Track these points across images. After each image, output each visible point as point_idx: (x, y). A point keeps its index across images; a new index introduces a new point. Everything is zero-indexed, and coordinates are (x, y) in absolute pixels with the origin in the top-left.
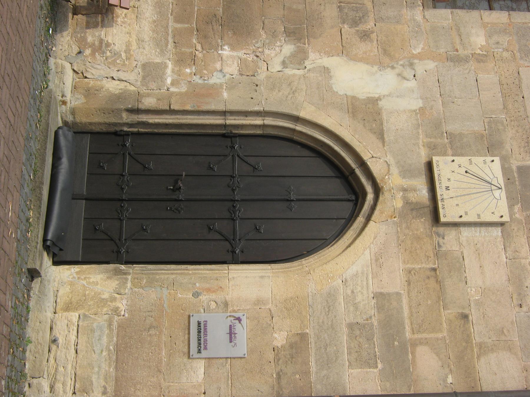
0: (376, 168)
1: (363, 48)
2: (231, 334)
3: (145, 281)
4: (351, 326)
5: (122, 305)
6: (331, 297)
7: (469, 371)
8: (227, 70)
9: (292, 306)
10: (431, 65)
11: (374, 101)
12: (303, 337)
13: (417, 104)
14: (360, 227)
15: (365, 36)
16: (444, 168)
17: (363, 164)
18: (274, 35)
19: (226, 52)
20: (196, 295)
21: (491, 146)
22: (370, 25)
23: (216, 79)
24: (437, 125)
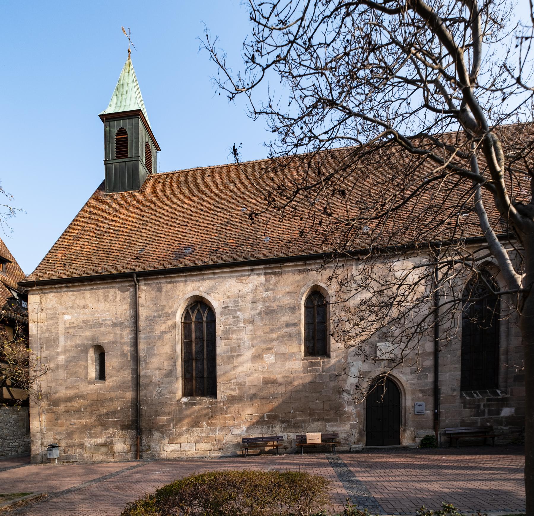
2: (420, 405)
4: (418, 380)
5: (412, 429)
6: (411, 384)
7: (429, 354)
8: (351, 409)
9: (413, 392)
12: (420, 390)
14: (382, 472)
18: (341, 398)
19: (346, 409)
20: (410, 413)
23: (354, 411)
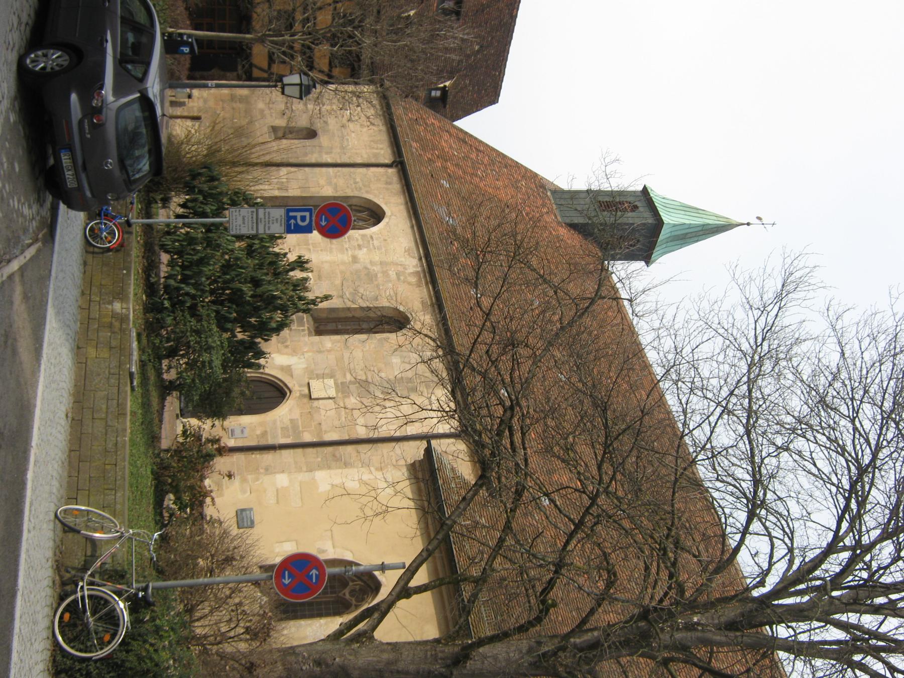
0: (290, 385)
1: (286, 350)
3: (835, 593)
6: (275, 422)
9: (261, 424)
10: (310, 354)
11: (290, 366)
12: (266, 432)
13: (304, 366)
15: (287, 347)
16: (313, 383)
17: (286, 385)
21: (332, 376)
22: (288, 343)
24: (312, 372)
